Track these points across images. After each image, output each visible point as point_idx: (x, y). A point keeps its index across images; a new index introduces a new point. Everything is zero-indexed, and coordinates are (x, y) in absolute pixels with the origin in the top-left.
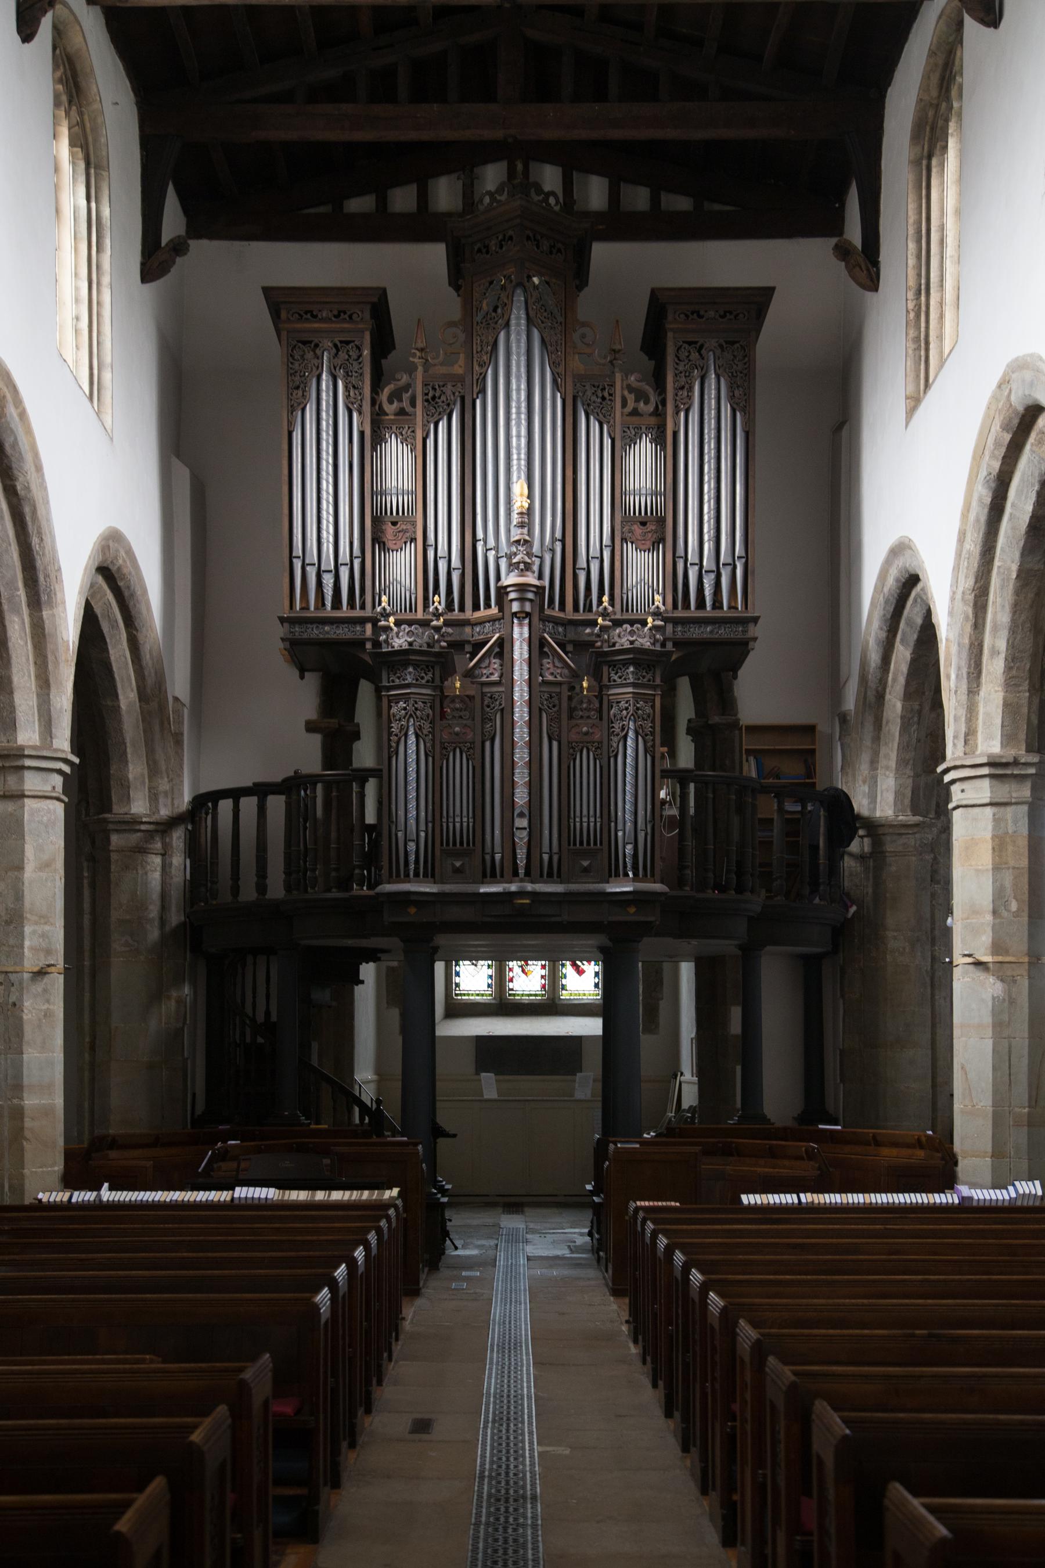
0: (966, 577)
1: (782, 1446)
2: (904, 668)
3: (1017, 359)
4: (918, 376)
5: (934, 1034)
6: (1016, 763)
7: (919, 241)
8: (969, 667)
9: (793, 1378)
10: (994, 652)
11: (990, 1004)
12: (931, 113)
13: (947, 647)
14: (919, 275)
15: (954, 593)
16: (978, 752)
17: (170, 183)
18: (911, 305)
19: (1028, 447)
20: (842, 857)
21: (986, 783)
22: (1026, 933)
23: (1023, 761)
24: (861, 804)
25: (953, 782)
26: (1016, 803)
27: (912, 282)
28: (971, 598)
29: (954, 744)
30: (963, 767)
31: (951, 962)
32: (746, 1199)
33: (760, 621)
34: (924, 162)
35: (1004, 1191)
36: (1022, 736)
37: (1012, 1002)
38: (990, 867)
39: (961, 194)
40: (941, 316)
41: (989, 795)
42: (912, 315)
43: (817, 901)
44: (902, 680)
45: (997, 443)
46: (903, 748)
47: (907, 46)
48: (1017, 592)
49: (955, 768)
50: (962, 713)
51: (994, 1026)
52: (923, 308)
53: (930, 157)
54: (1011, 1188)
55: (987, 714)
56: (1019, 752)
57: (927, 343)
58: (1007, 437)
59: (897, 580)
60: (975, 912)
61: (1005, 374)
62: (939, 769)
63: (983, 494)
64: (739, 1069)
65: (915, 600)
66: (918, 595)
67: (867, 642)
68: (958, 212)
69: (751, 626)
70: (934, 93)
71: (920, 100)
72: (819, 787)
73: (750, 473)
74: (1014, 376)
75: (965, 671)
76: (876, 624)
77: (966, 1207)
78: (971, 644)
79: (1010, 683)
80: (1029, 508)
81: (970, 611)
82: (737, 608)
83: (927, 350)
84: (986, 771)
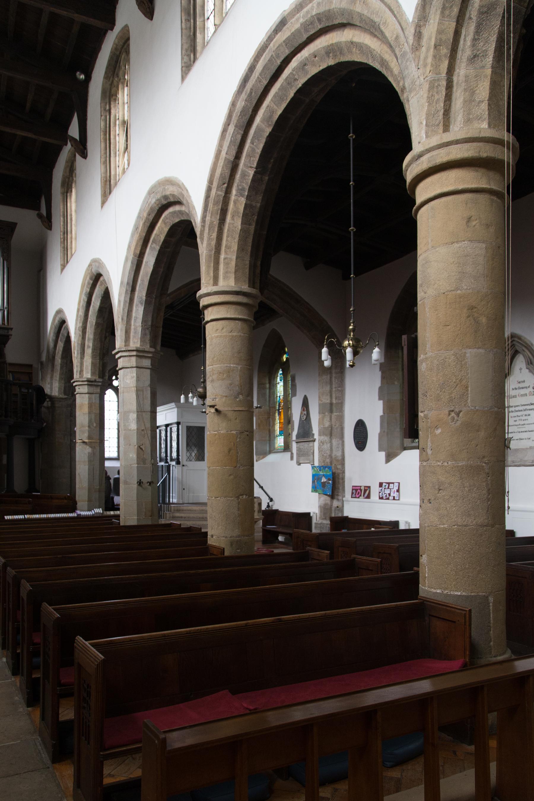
0: (80, 323)
1: (11, 595)
2: (61, 349)
3: (94, 259)
4: (64, 259)
5: (71, 464)
6: (95, 381)
7: (64, 218)
8: (81, 350)
9: (15, 573)
10: (89, 347)
11: (87, 455)
12: (67, 180)
13: (74, 344)
14: (64, 228)
15: (76, 327)
16: (84, 377)
17: (76, 115)
18: (62, 237)
19: (98, 286)
20: (41, 407)
21: (86, 387)
22: (98, 433)
23: (97, 380)
24: (47, 391)
25: (76, 386)
26: (95, 393)
27: (62, 230)
28: (81, 329)
29: (76, 374)
30: (79, 381)
31: (75, 442)
32: (6, 517)
33: (13, 330)
34: (65, 194)
35: (91, 512)
36: (97, 373)
37: (94, 454)
38: (87, 412)
39: (77, 206)
40: (71, 242)
41: (87, 390)
42: (62, 240)
43: (33, 421)
44: (60, 353)
45: (88, 283)
46: (61, 374)
47: (59, 158)
48: (95, 329)
49: (77, 381)
50: (79, 364)
51: (89, 461)
52: (66, 238)
53: (67, 193)
54: (93, 511)
55: (86, 365)
56: (96, 378)
57: (67, 249)
58: (91, 282)
59: (59, 321)
60: (83, 426)
61: (90, 263)
62: (72, 381)
63: (85, 298)
64: (6, 475)
65: (64, 328)
66: (65, 327)
67: (49, 340)
68: (76, 211)
69: (10, 331)
70: (68, 174)
71: (63, 175)
72: (34, 384)
73: (10, 281)
74: (93, 264)
75: (79, 352)
76: (52, 334)
77: (79, 517)
78: (81, 344)
79: (93, 356)
80: (99, 304)
81: (81, 333)
82: (5, 324)
83: (67, 251)
84: (86, 383)
